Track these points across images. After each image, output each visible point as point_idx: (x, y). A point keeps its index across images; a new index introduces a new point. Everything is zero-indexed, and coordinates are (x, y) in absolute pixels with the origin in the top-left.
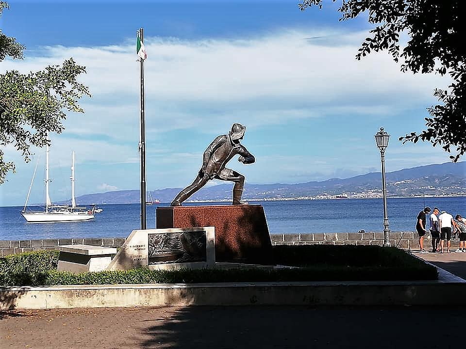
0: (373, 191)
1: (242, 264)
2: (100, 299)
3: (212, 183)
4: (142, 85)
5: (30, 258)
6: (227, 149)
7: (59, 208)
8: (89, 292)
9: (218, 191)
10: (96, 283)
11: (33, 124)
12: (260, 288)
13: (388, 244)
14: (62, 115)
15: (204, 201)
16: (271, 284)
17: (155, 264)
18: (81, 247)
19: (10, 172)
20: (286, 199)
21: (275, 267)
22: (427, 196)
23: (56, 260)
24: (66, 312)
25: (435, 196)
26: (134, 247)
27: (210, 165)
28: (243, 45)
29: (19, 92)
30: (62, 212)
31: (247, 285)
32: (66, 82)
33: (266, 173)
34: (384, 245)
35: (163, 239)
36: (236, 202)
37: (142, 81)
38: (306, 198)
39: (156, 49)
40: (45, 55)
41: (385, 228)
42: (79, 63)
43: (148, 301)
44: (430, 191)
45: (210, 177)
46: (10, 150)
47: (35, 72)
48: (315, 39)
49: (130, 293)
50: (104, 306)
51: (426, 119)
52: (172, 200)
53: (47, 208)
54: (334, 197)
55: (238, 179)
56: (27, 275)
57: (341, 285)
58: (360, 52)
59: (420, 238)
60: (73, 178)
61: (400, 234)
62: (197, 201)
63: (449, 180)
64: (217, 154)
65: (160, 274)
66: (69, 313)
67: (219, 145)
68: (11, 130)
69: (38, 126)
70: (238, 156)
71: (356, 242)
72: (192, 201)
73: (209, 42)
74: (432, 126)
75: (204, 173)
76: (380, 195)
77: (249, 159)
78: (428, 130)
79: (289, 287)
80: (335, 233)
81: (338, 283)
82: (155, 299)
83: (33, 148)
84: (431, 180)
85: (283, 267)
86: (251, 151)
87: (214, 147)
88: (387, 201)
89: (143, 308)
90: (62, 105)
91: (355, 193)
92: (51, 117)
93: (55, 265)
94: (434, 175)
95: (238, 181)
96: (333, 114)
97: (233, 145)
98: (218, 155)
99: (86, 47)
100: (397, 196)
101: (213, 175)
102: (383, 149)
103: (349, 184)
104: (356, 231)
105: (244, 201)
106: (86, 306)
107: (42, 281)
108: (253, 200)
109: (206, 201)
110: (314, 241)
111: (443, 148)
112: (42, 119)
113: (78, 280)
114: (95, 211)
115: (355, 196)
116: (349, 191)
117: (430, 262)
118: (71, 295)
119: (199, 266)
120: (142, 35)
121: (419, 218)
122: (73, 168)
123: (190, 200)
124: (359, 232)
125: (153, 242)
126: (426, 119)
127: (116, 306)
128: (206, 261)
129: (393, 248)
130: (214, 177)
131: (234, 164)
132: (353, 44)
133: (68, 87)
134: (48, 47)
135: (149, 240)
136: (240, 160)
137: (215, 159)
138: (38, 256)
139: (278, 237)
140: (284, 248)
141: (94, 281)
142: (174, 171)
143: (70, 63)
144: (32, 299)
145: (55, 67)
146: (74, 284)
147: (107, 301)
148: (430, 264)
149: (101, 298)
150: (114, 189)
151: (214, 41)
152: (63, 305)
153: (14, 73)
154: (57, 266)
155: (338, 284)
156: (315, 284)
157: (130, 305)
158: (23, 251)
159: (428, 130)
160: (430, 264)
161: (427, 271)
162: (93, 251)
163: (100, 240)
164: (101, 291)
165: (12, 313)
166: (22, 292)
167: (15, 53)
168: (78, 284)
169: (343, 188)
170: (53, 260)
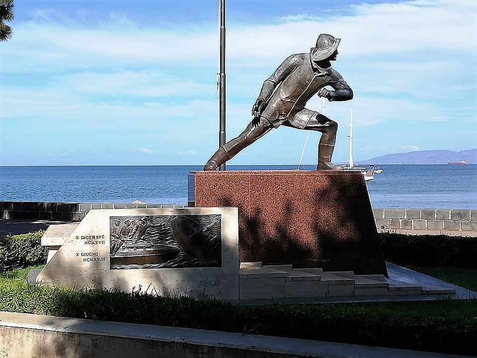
3: (280, 132)
9: (289, 148)
26: (83, 238)
31: (169, 339)
86: (349, 79)
98: (288, 86)
99: (390, 3)
122: (351, 125)
125: (119, 230)
128: (219, 265)
134: (352, 6)
150: (416, 148)
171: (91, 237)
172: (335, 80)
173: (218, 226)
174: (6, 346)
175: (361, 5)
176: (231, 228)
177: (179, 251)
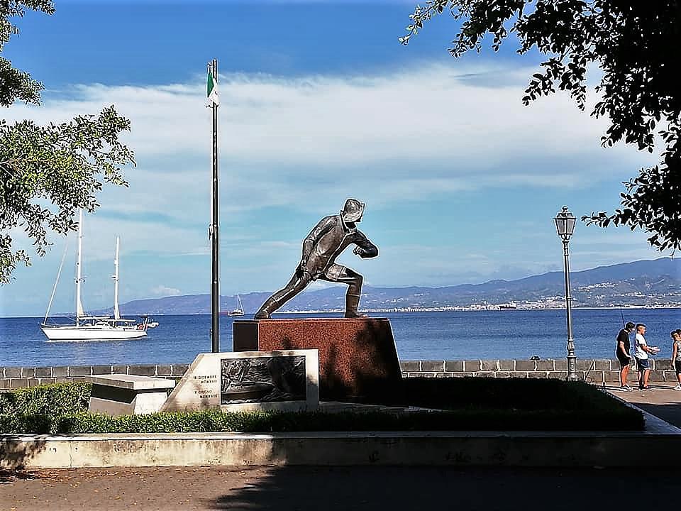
0: (553, 298)
1: (358, 405)
2: (150, 454)
3: (316, 285)
4: (215, 141)
5: (49, 393)
6: (339, 236)
8: (133, 443)
9: (324, 296)
10: (144, 430)
11: (54, 198)
12: (384, 441)
14: (95, 184)
15: (306, 312)
16: (399, 434)
18: (125, 378)
19: (19, 265)
20: (427, 310)
21: (406, 410)
22: (633, 307)
23: (87, 396)
25: (645, 307)
27: (313, 260)
28: (365, 85)
30: (99, 326)
34: (567, 378)
35: (242, 367)
36: (350, 313)
37: (215, 137)
38: (456, 308)
39: (236, 91)
40: (77, 98)
41: (570, 353)
42: (121, 113)
43: (220, 457)
45: (312, 277)
46: (18, 233)
48: (470, 77)
49: (193, 445)
50: (155, 464)
51: (623, 195)
52: (256, 310)
53: (77, 320)
54: (497, 307)
55: (354, 279)
56: (45, 418)
58: (529, 94)
59: (622, 369)
60: (117, 277)
61: (588, 363)
63: (666, 284)
64: (323, 244)
66: (104, 474)
67: (326, 230)
68: (21, 207)
71: (526, 374)
72: (288, 312)
73: (315, 80)
74: (629, 206)
75: (303, 271)
76: (563, 305)
77: (368, 251)
78: (624, 210)
79: (424, 439)
80: (495, 360)
81: (498, 434)
82: (234, 457)
83: (51, 234)
84: (639, 284)
85: (416, 409)
87: (318, 234)
91: (527, 302)
93: (85, 404)
94: (643, 276)
95: (353, 284)
96: (496, 185)
97: (346, 230)
101: (317, 274)
102: (566, 238)
103: (518, 289)
105: (363, 309)
106: (128, 464)
107: (66, 428)
108: (378, 311)
109: (310, 312)
110: (465, 371)
111: (649, 240)
112: (68, 191)
113: (118, 426)
114: (148, 325)
115: (528, 305)
116: (519, 300)
117: (635, 404)
118: (107, 448)
121: (619, 339)
122: (116, 262)
123: (285, 309)
124: (532, 359)
125: (227, 372)
126: (623, 195)
127: (173, 464)
129: (581, 383)
130: (317, 276)
131: (349, 258)
132: (515, 83)
133: (106, 148)
134: (81, 86)
135: (222, 367)
136: (356, 253)
137: (321, 251)
138: (61, 391)
140: (421, 381)
141: (142, 428)
142: (261, 268)
143: (109, 115)
144: (57, 454)
145: (88, 118)
146: (112, 432)
147: (159, 458)
149: (151, 452)
150: (175, 292)
151: (321, 79)
152: (96, 462)
153: (26, 125)
155: (499, 436)
156: (463, 434)
157: (192, 463)
158: (40, 383)
159: (624, 210)
160: (635, 407)
161: (629, 417)
162: (140, 383)
163: (152, 368)
164: (151, 443)
166: (38, 445)
167: (28, 96)
168: (118, 432)
169: (510, 294)
170: (83, 396)
171: (197, 377)
172: (360, 240)
174: (219, 455)
175: (91, 86)
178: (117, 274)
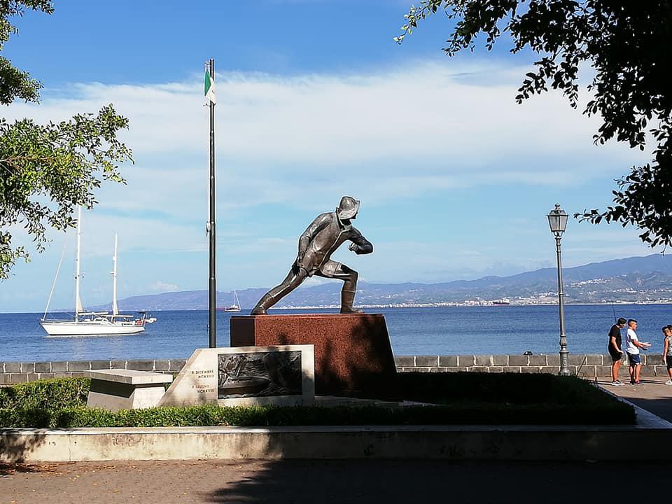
0: (546, 294)
1: (354, 400)
3: (312, 281)
6: (336, 233)
7: (94, 316)
9: (319, 293)
10: (142, 424)
13: (566, 371)
14: (95, 181)
16: (393, 428)
17: (228, 398)
21: (401, 404)
22: (625, 303)
23: (85, 390)
24: (100, 467)
25: (636, 303)
29: (32, 148)
32: (102, 139)
33: (392, 269)
34: (559, 373)
35: (239, 362)
36: (346, 308)
39: (232, 90)
41: (562, 348)
44: (628, 296)
46: (17, 229)
47: (57, 123)
50: (153, 458)
51: (614, 192)
52: (252, 306)
54: (490, 303)
55: (349, 275)
57: (496, 430)
58: (522, 93)
59: (614, 364)
60: (115, 273)
61: (583, 358)
62: (292, 307)
65: (233, 413)
66: (103, 468)
68: (20, 204)
69: (60, 199)
70: (348, 243)
72: (285, 308)
74: (621, 203)
75: (299, 267)
76: (555, 301)
77: (363, 247)
80: (489, 354)
81: (491, 428)
82: (229, 450)
83: (50, 230)
84: (630, 280)
85: (411, 403)
86: (366, 235)
88: (564, 309)
89: (207, 462)
90: (93, 167)
92: (79, 184)
93: (84, 398)
98: (320, 241)
100: (581, 302)
102: (558, 235)
104: (520, 351)
105: (358, 305)
106: (126, 457)
107: (65, 422)
110: (458, 366)
113: (116, 420)
116: (512, 295)
118: (106, 442)
119: (285, 400)
120: (212, 69)
121: (611, 335)
122: (115, 258)
123: (282, 305)
124: (525, 354)
125: (225, 368)
126: (614, 192)
129: (573, 378)
131: (344, 255)
133: (105, 146)
134: (79, 85)
135: (219, 362)
136: (351, 249)
137: (316, 247)
138: (60, 386)
139: (407, 361)
140: (415, 375)
141: (140, 422)
142: (256, 265)
143: (108, 113)
144: (56, 447)
145: (87, 116)
146: (111, 426)
148: (624, 400)
149: (149, 446)
150: (172, 288)
152: (94, 455)
153: (26, 123)
154: (87, 399)
157: (189, 457)
158: (39, 378)
161: (621, 411)
162: (138, 378)
163: (150, 363)
165: (22, 467)
166: (38, 439)
167: (28, 94)
168: (116, 426)
170: (82, 391)
172: (356, 237)
173: (299, 361)
176: (309, 364)
177: (269, 382)
178: (115, 270)
